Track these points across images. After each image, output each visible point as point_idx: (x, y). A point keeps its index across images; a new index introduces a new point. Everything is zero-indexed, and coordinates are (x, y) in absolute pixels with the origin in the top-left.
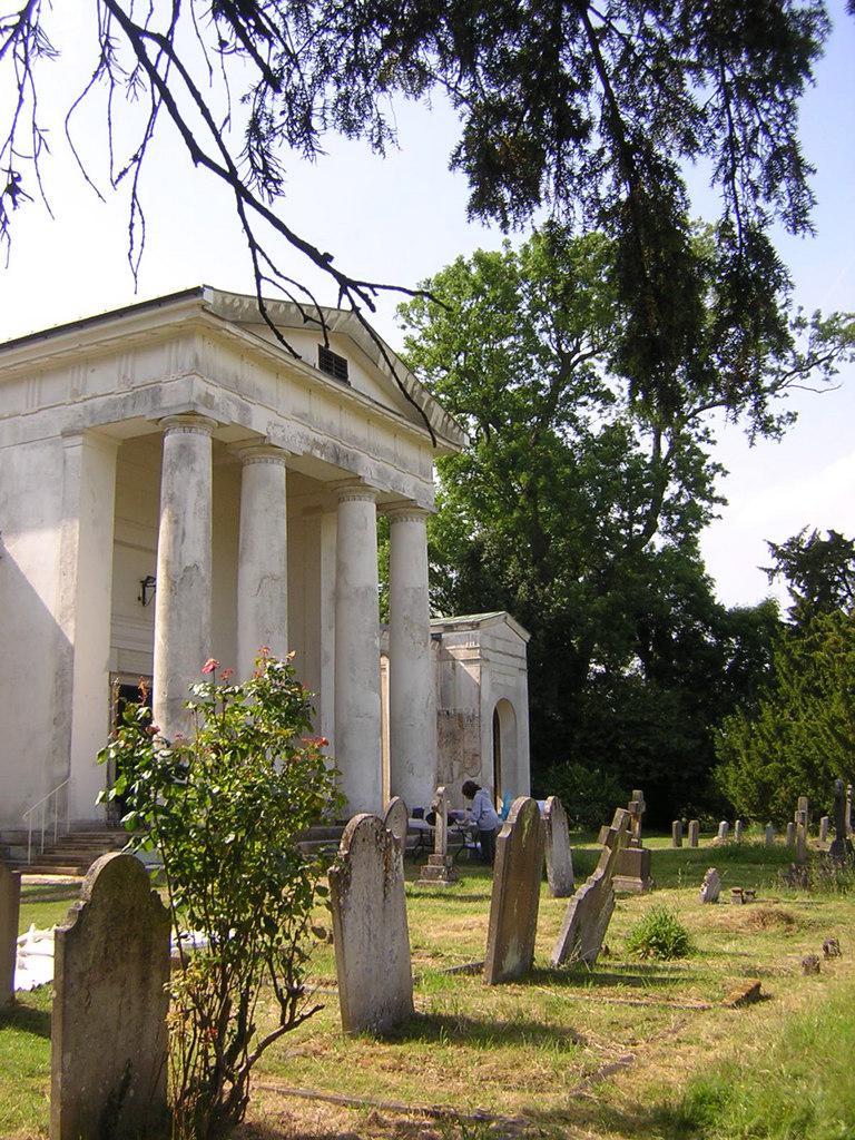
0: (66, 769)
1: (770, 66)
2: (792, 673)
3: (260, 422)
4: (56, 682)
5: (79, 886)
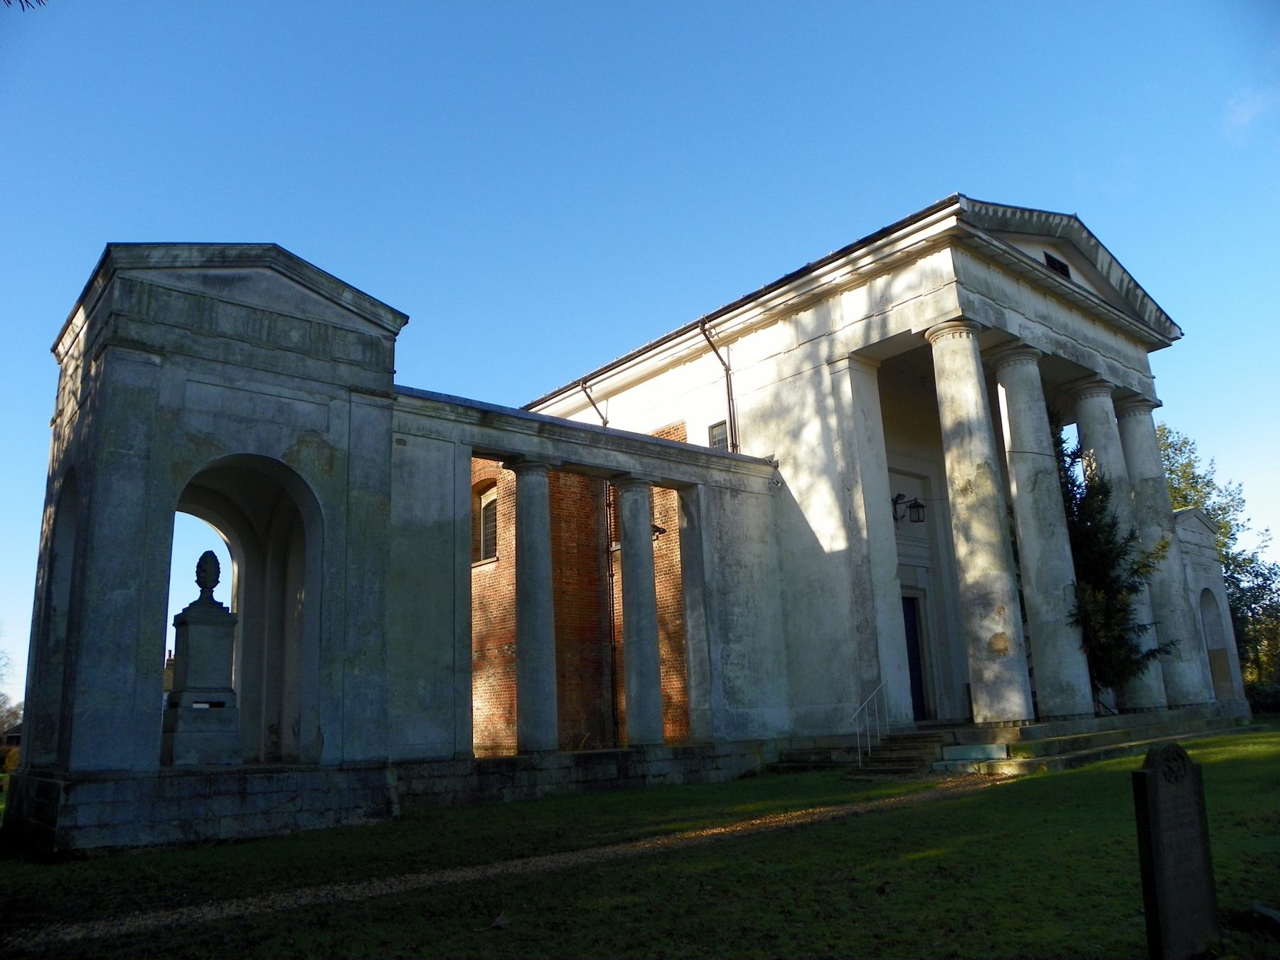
0: (875, 673)
2: (159, 921)
4: (854, 590)
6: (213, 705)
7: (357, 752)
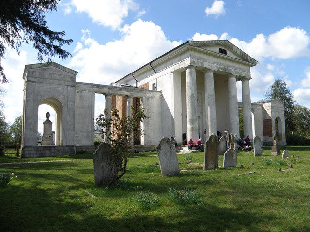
3: (206, 65)
5: (271, 136)
7: (69, 144)
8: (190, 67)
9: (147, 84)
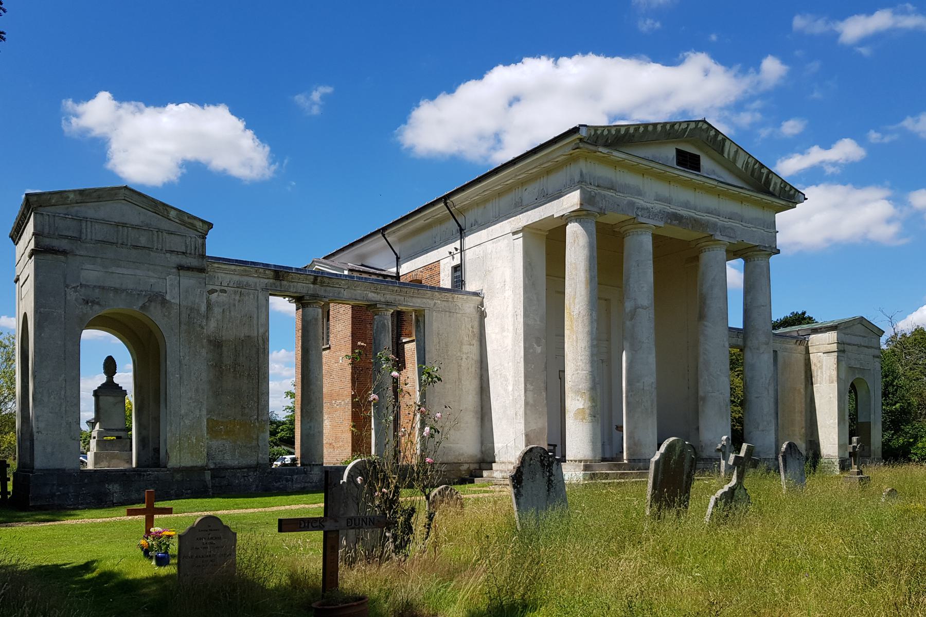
1: (88, 589)
6: (118, 438)
8: (575, 216)
9: (434, 268)
